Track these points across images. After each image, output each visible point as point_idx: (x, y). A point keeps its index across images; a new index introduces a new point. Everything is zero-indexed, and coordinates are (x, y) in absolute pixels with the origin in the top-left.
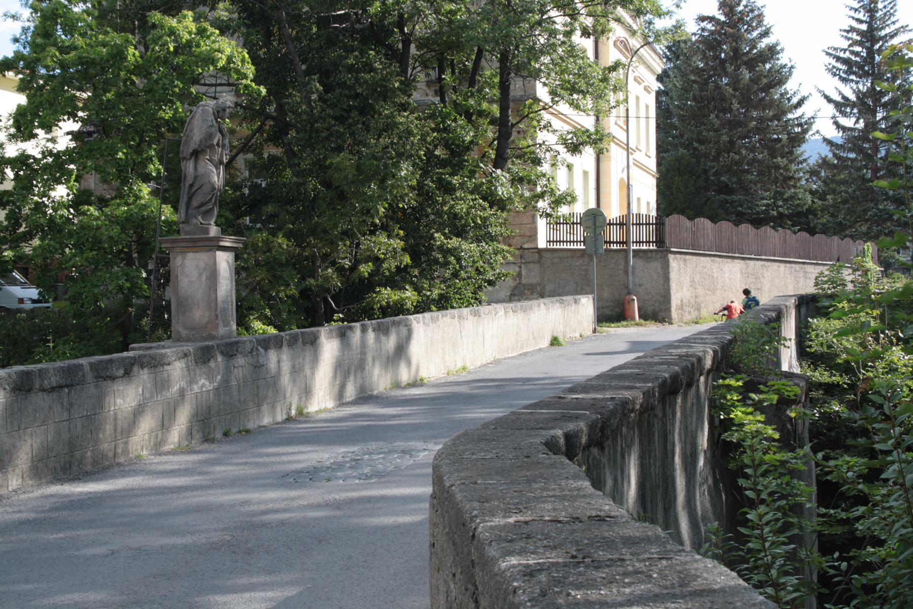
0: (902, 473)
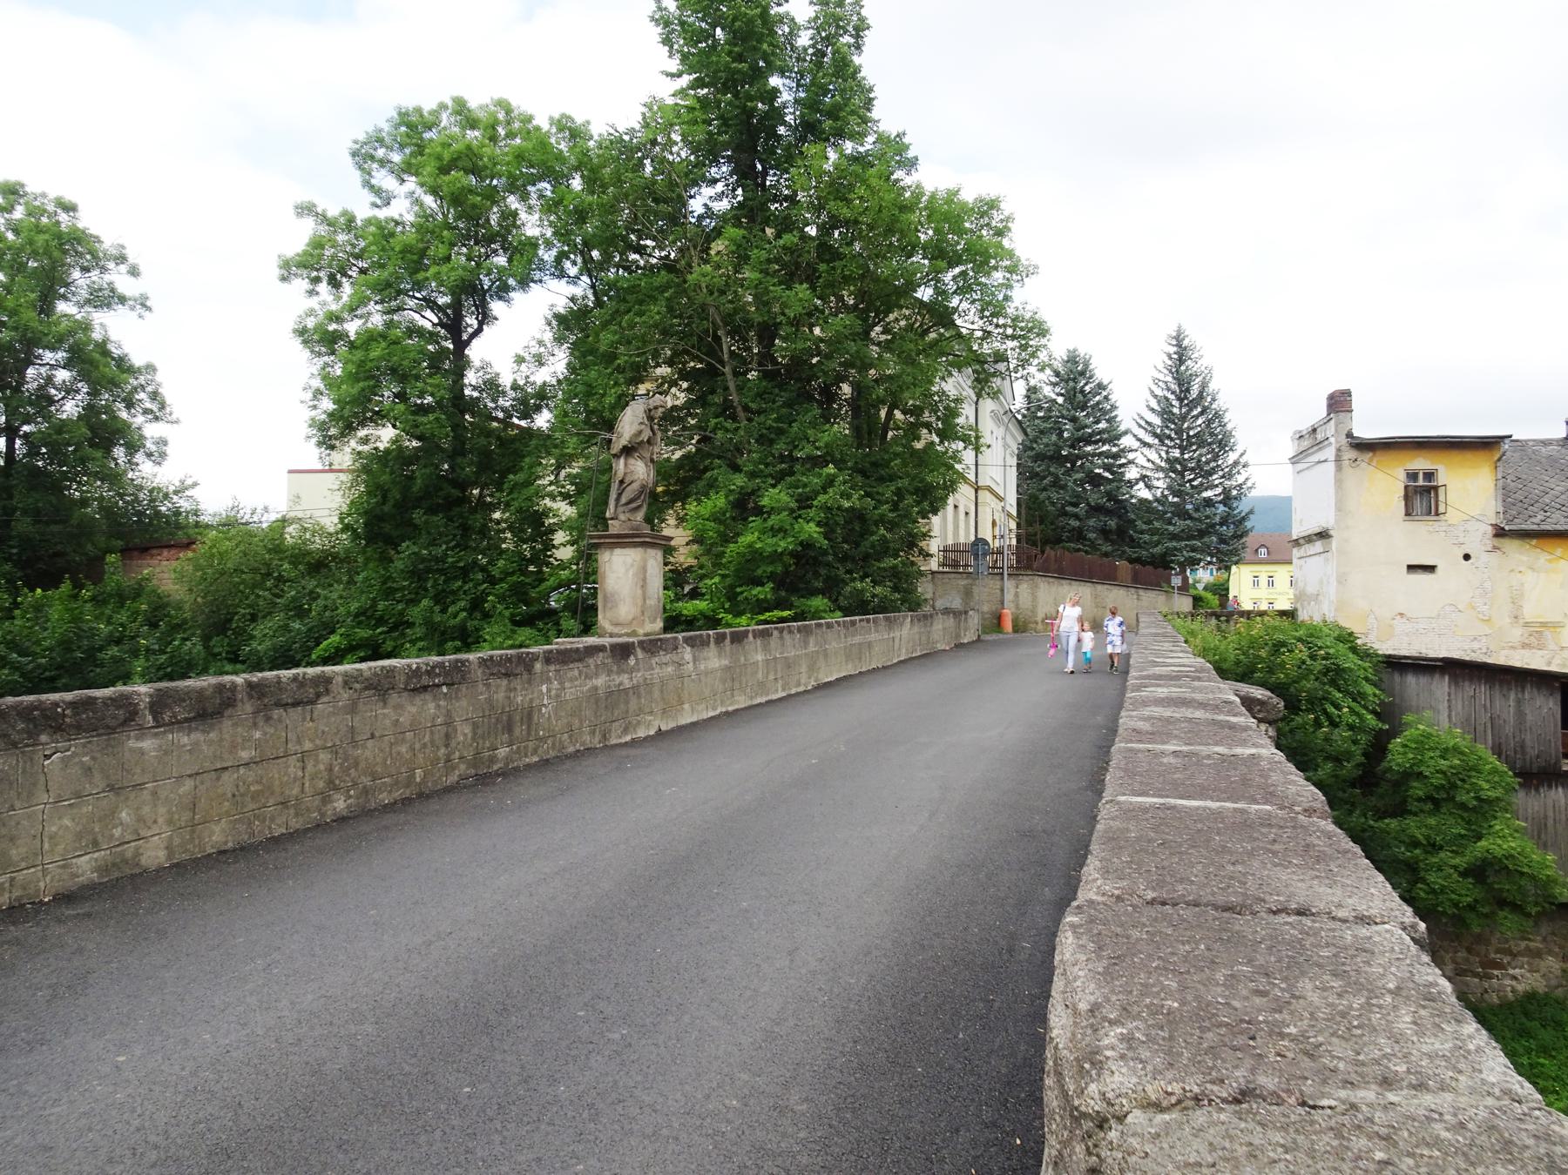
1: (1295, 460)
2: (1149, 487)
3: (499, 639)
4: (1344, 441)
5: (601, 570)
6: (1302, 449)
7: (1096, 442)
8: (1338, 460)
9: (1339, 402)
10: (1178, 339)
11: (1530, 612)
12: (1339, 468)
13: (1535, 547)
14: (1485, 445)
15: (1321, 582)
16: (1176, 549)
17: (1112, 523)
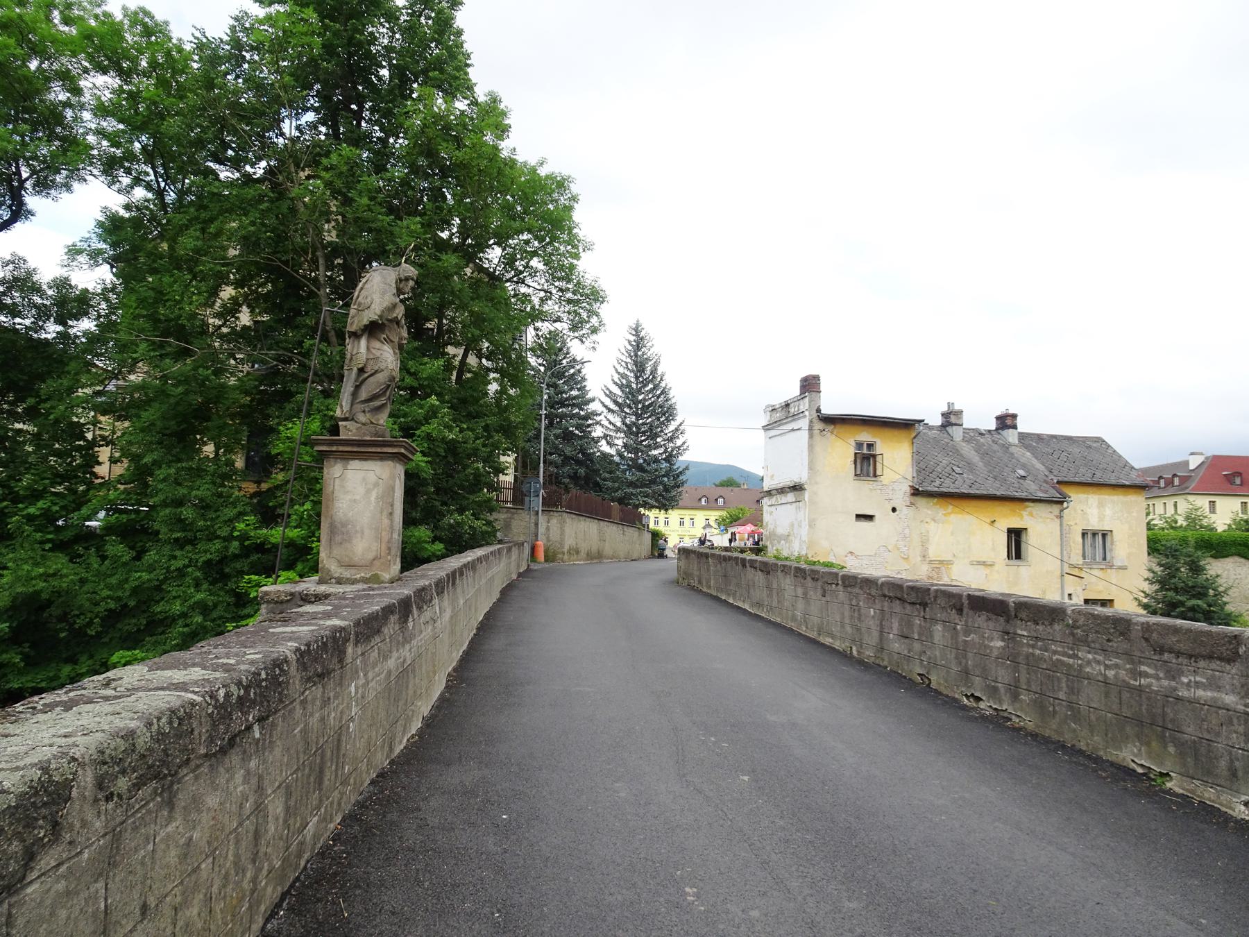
0: (144, 123)
1: (767, 428)
2: (610, 444)
3: (26, 567)
4: (815, 415)
5: (327, 490)
6: (774, 420)
7: (568, 406)
8: (811, 429)
9: (810, 385)
10: (637, 330)
11: (933, 554)
12: (811, 436)
13: (934, 504)
14: (905, 425)
15: (792, 525)
16: (632, 494)
17: (582, 471)
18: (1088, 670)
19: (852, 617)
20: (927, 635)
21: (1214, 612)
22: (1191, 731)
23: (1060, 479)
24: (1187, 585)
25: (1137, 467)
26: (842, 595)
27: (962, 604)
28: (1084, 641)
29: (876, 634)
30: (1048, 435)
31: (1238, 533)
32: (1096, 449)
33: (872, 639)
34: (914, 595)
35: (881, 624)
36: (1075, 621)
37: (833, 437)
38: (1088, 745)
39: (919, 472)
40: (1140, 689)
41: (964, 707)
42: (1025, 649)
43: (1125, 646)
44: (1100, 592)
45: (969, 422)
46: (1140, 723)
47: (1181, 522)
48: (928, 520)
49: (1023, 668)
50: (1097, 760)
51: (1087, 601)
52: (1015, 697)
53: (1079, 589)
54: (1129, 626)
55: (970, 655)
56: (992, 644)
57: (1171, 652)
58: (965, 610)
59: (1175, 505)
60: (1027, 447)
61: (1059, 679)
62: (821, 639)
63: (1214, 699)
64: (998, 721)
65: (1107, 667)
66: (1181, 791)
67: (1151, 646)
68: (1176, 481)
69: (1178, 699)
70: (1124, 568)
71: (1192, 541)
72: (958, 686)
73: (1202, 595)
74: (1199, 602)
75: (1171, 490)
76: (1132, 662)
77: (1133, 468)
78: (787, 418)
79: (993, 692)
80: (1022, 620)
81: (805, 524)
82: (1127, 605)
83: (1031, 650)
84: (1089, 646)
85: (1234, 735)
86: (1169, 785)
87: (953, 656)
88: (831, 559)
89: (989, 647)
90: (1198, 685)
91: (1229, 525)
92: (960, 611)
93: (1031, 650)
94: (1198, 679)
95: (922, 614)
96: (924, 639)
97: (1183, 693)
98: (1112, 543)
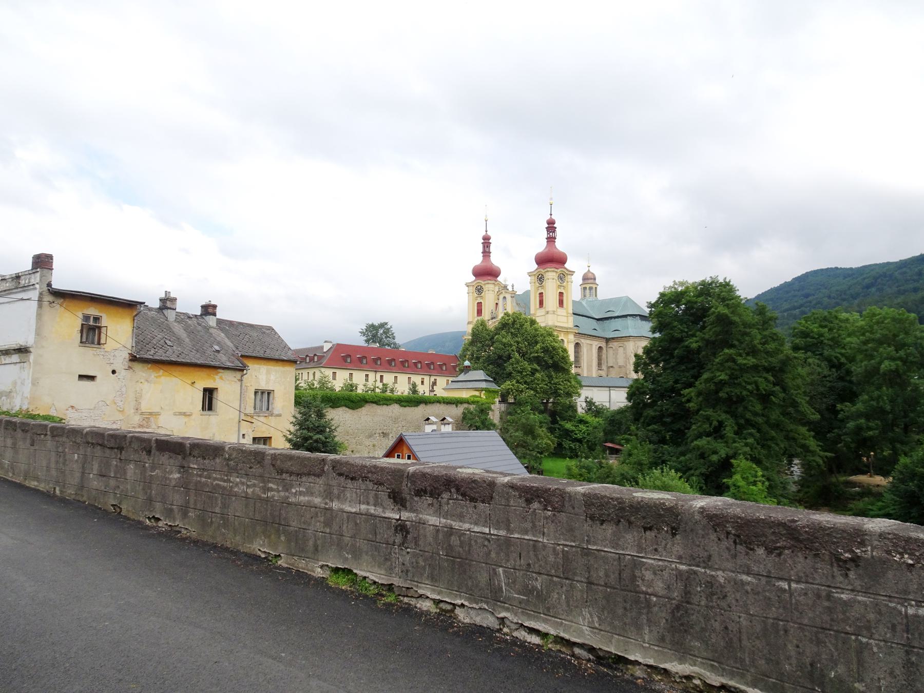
4: (45, 288)
8: (40, 300)
11: (144, 407)
12: (40, 306)
13: (148, 369)
15: (15, 383)
18: (236, 489)
19: (57, 462)
20: (121, 473)
21: (328, 442)
22: (295, 524)
23: (243, 354)
24: (314, 425)
25: (292, 349)
26: (50, 444)
27: (151, 447)
28: (234, 470)
29: (77, 475)
30: (236, 322)
31: (347, 392)
32: (268, 335)
33: (74, 479)
34: (113, 440)
35: (83, 467)
36: (230, 455)
37: (62, 309)
38: (232, 543)
39: (137, 343)
40: (267, 500)
41: (147, 528)
42: (195, 478)
43: (260, 470)
44: (264, 432)
45: (180, 307)
46: (265, 522)
47: (316, 385)
48: (142, 381)
49: (192, 492)
50: (236, 553)
51: (255, 440)
52: (185, 515)
53: (250, 431)
54: (264, 457)
55: (154, 486)
56: (171, 476)
57: (287, 473)
58: (153, 451)
59: (314, 374)
60: (222, 330)
61: (216, 498)
62: (27, 483)
63: (309, 502)
64: (172, 535)
65: (248, 486)
66: (286, 566)
67: (276, 470)
68: (316, 358)
69: (289, 504)
70: (279, 415)
71: (319, 396)
72: (143, 511)
73: (322, 432)
74: (321, 436)
75: (312, 364)
76: (264, 482)
77: (289, 348)
78: (17, 288)
79: (169, 513)
80: (194, 456)
81: (28, 383)
82: (280, 444)
83: (199, 479)
84: (237, 473)
85: (318, 524)
86: (279, 563)
87: (141, 487)
88: (53, 413)
89: (169, 478)
90: (301, 493)
91: (342, 388)
92: (149, 452)
93: (199, 479)
94: (301, 489)
95: (119, 456)
96: (119, 476)
97: (292, 500)
98: (273, 399)
